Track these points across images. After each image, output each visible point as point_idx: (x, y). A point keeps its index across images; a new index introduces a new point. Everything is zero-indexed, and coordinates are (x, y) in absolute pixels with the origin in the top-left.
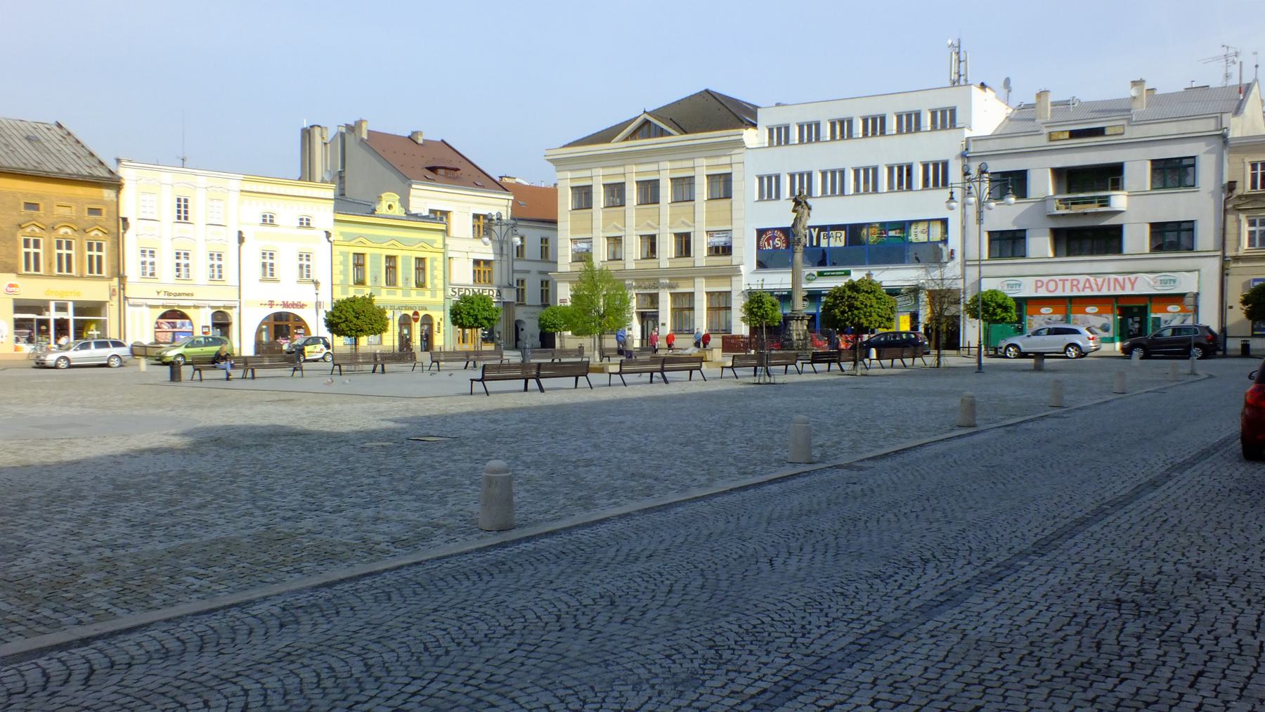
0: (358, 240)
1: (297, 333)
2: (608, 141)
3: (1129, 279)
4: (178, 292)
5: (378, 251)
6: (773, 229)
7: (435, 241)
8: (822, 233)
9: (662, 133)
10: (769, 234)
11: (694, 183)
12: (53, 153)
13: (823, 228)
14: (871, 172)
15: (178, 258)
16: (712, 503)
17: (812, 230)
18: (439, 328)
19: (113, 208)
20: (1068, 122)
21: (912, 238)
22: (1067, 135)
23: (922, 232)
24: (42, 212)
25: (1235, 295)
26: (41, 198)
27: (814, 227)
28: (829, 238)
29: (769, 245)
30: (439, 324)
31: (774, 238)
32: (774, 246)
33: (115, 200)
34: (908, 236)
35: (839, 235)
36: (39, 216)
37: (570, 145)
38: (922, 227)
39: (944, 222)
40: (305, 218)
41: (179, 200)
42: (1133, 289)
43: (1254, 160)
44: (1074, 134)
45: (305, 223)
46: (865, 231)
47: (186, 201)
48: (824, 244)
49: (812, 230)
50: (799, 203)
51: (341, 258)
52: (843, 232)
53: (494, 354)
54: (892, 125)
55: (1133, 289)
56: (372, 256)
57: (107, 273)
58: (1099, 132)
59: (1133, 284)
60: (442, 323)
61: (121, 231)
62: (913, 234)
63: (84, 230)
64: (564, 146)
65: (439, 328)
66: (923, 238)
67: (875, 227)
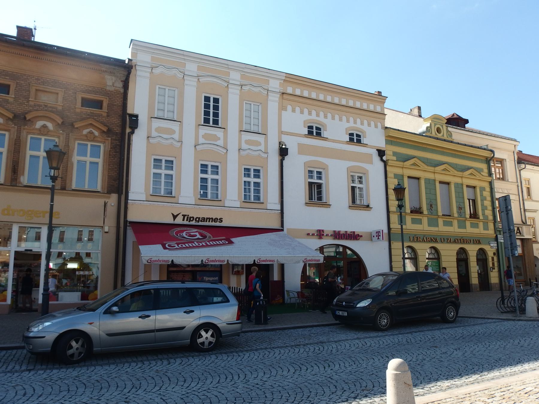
4: (201, 216)
15: (204, 171)
18: (493, 264)
19: (119, 102)
24: (12, 94)
26: (13, 76)
30: (493, 258)
33: (122, 91)
36: (7, 101)
40: (355, 133)
41: (207, 99)
47: (216, 101)
53: (44, 290)
56: (427, 181)
57: (102, 188)
61: (128, 130)
63: (72, 125)
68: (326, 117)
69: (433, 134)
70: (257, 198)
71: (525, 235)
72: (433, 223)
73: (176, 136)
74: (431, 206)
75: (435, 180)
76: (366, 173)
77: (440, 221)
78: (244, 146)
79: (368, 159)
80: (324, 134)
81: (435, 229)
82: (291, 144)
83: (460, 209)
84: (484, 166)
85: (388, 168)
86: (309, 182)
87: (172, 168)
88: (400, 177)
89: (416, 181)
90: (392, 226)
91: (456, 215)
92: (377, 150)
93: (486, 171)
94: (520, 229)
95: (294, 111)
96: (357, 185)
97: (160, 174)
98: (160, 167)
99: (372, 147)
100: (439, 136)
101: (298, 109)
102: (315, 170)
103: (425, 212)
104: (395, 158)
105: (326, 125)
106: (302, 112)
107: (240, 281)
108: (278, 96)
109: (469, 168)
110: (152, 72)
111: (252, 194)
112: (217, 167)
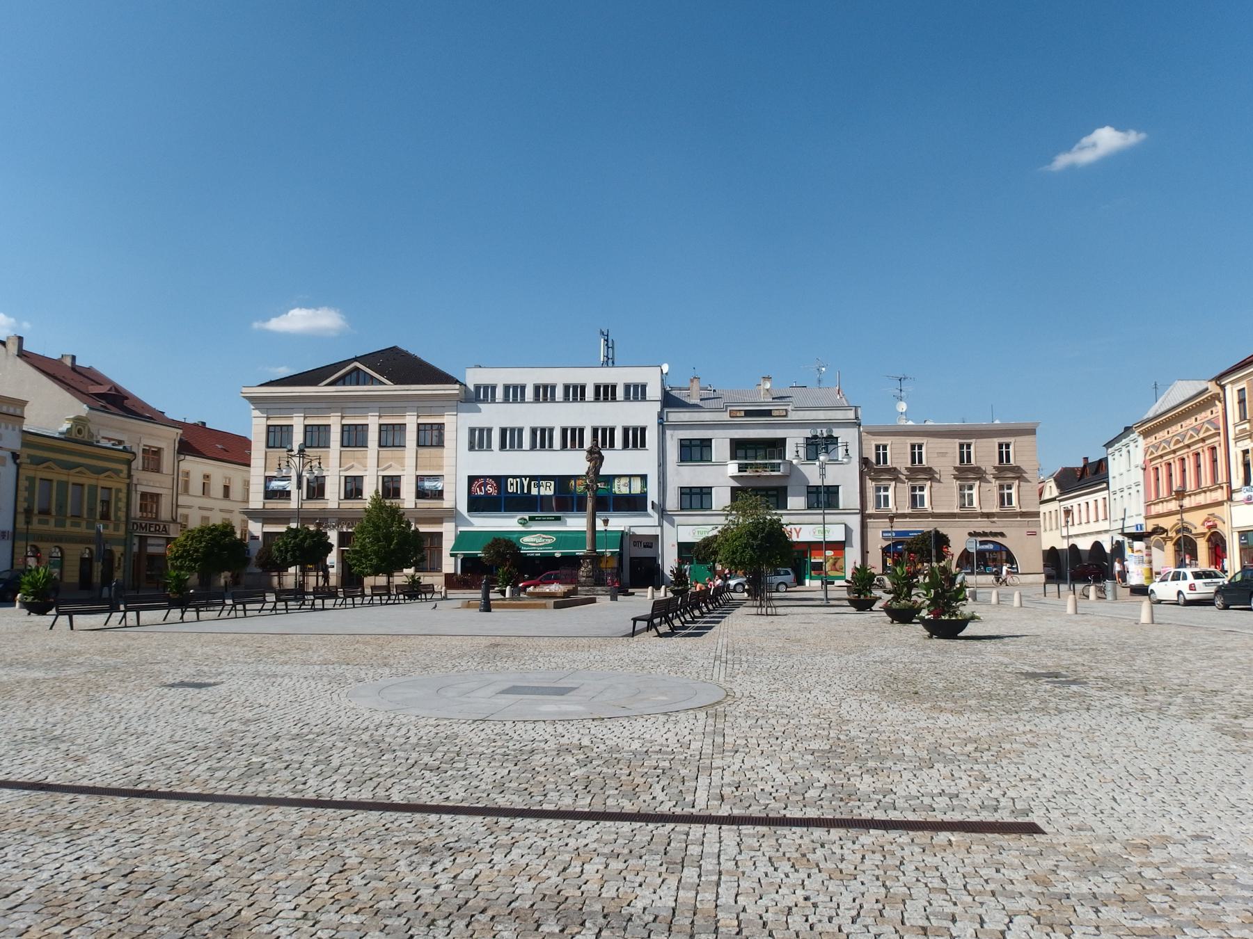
0: (45, 465)
1: (317, 576)
2: (315, 383)
3: (795, 529)
5: (64, 478)
7: (121, 471)
8: (533, 483)
10: (482, 481)
13: (532, 478)
14: (538, 433)
17: (523, 479)
18: (119, 564)
20: (744, 403)
21: (616, 490)
22: (743, 414)
23: (624, 486)
25: (877, 542)
27: (525, 477)
28: (539, 487)
29: (481, 490)
30: (120, 559)
31: (485, 485)
32: (486, 492)
35: (548, 484)
38: (624, 481)
39: (644, 478)
42: (798, 537)
43: (878, 443)
44: (748, 413)
46: (573, 482)
48: (534, 491)
49: (523, 479)
51: (26, 483)
52: (553, 483)
54: (590, 393)
55: (798, 537)
56: (59, 483)
58: (768, 413)
59: (798, 533)
60: (122, 559)
62: (616, 486)
65: (119, 564)
66: (625, 491)
69: (73, 436)
72: (60, 523)
74: (61, 507)
75: (97, 486)
77: (68, 522)
81: (62, 529)
83: (92, 510)
84: (124, 468)
85: (20, 470)
88: (31, 480)
90: (17, 526)
93: (125, 472)
100: (80, 437)
101: (10, 426)
103: (54, 513)
109: (107, 470)
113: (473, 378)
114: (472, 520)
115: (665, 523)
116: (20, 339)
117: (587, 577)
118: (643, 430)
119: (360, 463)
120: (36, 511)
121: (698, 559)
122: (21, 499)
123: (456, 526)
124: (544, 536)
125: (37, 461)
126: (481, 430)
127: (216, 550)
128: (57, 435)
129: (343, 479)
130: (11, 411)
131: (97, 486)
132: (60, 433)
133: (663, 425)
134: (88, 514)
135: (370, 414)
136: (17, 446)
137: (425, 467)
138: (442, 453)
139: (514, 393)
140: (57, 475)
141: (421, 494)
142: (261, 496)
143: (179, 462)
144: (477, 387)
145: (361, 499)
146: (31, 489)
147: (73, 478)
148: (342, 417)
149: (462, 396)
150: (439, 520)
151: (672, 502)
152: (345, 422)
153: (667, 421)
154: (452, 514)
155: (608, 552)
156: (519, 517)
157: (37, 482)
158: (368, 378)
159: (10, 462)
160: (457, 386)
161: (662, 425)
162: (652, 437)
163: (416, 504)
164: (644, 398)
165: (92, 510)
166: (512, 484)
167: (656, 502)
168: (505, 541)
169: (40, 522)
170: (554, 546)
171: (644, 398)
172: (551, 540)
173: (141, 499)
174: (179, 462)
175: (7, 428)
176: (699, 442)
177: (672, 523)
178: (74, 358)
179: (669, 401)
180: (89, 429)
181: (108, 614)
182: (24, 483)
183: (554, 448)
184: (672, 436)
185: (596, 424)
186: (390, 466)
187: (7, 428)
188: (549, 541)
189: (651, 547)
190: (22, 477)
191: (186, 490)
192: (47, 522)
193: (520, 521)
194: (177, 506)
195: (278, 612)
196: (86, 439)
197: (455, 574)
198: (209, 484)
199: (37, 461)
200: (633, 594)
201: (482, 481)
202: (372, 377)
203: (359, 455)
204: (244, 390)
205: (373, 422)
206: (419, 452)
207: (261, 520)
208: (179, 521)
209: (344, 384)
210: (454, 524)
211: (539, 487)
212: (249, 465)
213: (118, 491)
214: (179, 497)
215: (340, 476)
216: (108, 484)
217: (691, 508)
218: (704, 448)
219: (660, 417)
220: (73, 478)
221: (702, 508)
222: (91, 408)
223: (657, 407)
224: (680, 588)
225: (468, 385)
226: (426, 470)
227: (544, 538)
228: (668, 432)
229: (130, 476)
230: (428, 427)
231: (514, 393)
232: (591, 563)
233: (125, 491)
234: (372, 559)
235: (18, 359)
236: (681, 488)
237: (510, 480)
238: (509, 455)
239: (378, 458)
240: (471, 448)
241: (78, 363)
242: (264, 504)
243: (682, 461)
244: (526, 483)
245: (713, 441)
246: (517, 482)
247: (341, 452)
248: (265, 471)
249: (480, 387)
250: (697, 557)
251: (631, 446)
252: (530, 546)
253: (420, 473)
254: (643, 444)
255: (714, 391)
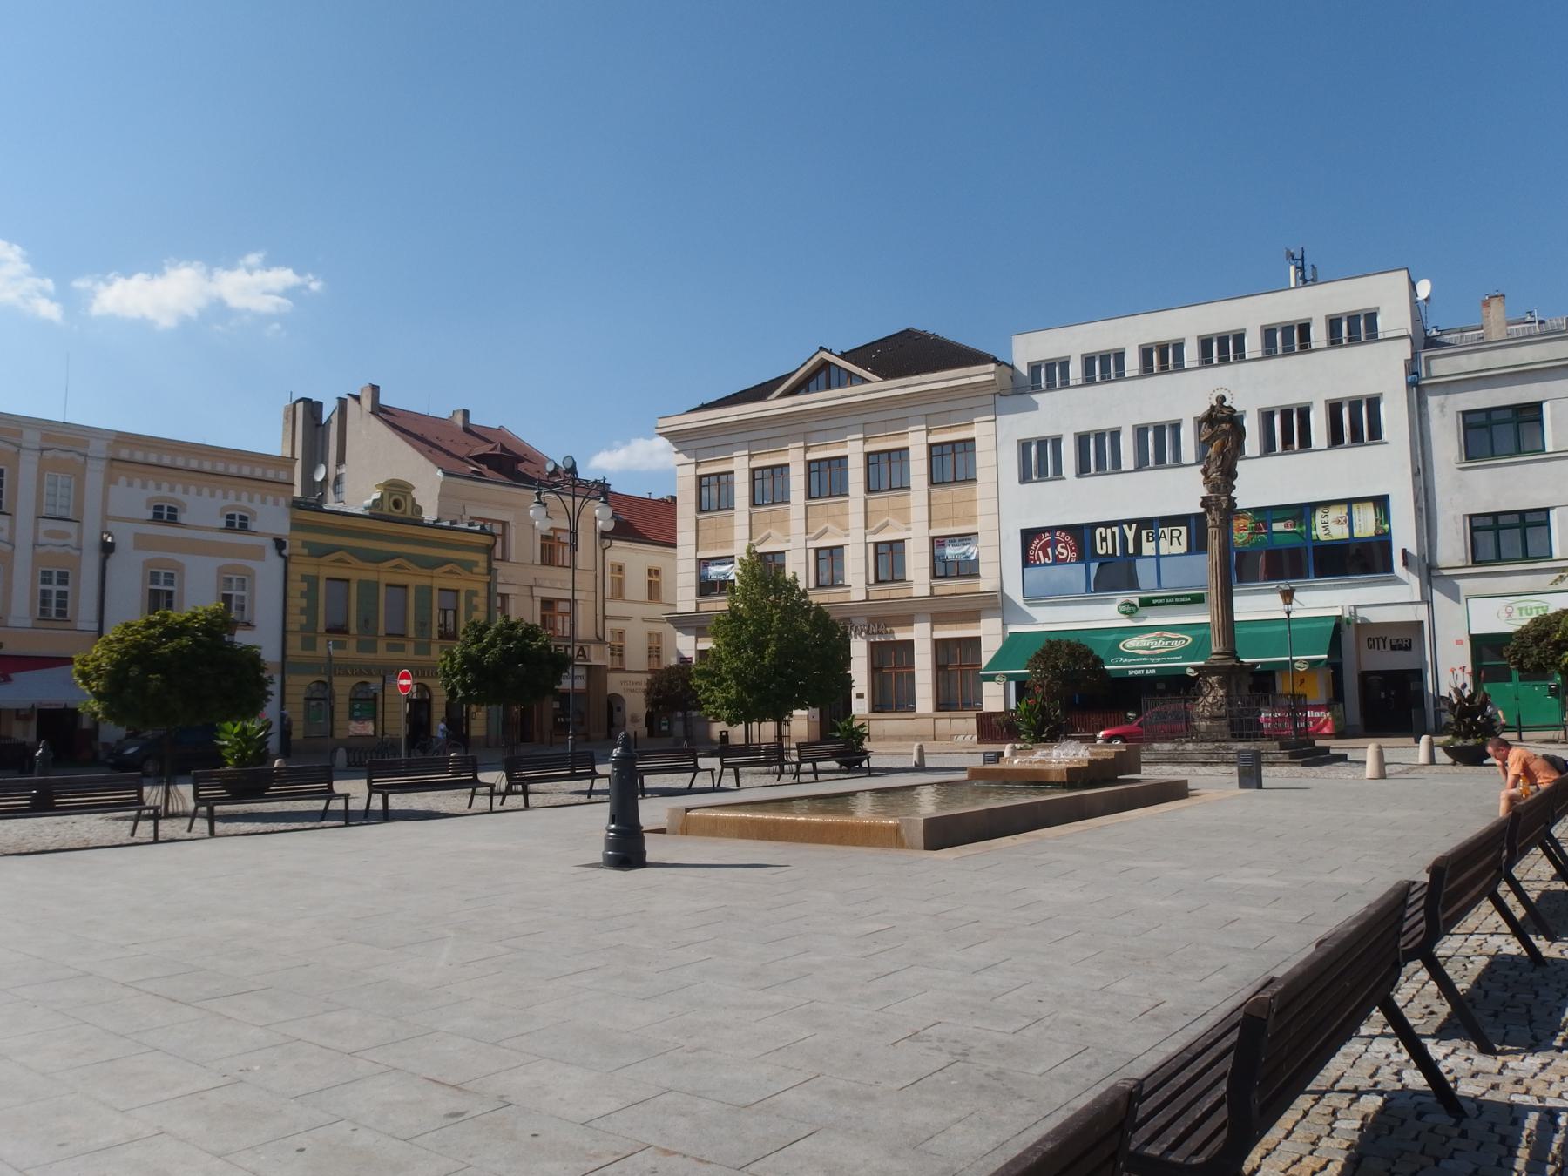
6: (1052, 529)
7: (476, 564)
8: (1144, 533)
9: (852, 378)
11: (974, 450)
12: (1400, 773)
13: (1144, 523)
14: (1277, 419)
16: (436, 747)
17: (1125, 527)
21: (1320, 533)
23: (1338, 522)
27: (1129, 522)
28: (1157, 539)
29: (1046, 555)
34: (1309, 529)
35: (1176, 533)
37: (704, 407)
38: (1336, 513)
39: (1381, 503)
40: (237, 513)
45: (237, 523)
49: (1125, 527)
50: (1222, 474)
52: (1184, 529)
54: (1319, 334)
56: (419, 589)
64: (689, 412)
66: (1339, 532)
67: (1247, 518)
68: (186, 491)
69: (386, 511)
70: (62, 613)
71: (592, 659)
72: (367, 646)
73: (72, 541)
74: (367, 623)
75: (431, 588)
76: (251, 574)
77: (381, 645)
78: (43, 539)
79: (258, 553)
80: (182, 518)
81: (372, 656)
82: (122, 535)
83: (423, 626)
84: (481, 558)
85: (291, 567)
86: (151, 590)
87: (66, 583)
88: (312, 581)
89: (345, 583)
90: (289, 652)
91: (412, 633)
92: (275, 539)
93: (483, 564)
94: (586, 649)
95: (130, 485)
96: (235, 593)
97: (50, 591)
98: (50, 582)
99: (264, 535)
100: (397, 512)
101: (270, 499)
102: (162, 572)
103: (353, 629)
104: (305, 551)
105: (185, 505)
106: (144, 486)
107: (898, 616)
108: (103, 463)
109: (447, 561)
110: (41, 458)
111: (54, 608)
112: (172, 576)
113: (1026, 350)
114: (1032, 611)
115: (1438, 597)
116: (375, 389)
117: (1214, 718)
118: (1374, 403)
119: (839, 525)
120: (321, 628)
121: (1521, 669)
122: (293, 609)
123: (1004, 625)
124: (1169, 635)
125: (319, 552)
126: (1042, 443)
127: (134, 671)
128: (360, 511)
129: (812, 554)
130: (271, 475)
131: (431, 588)
132: (366, 508)
133: (1418, 386)
134: (416, 630)
135: (849, 437)
136: (283, 528)
137: (944, 521)
138: (974, 491)
139: (1102, 367)
140: (358, 572)
141: (941, 568)
142: (693, 591)
143: (604, 550)
144: (1034, 368)
145: (842, 585)
146: (311, 594)
147: (386, 575)
148: (807, 449)
149: (1008, 384)
150: (973, 616)
151: (1452, 547)
152: (811, 456)
153: (1429, 377)
154: (996, 604)
155: (1301, 659)
156: (1119, 601)
157: (322, 584)
158: (844, 374)
159: (271, 552)
160: (992, 367)
161: (1418, 386)
162: (1394, 417)
163: (932, 588)
164: (1373, 336)
165: (423, 626)
166: (1104, 539)
167: (1413, 549)
168: (1069, 644)
169: (390, 648)
170: (1186, 653)
171: (1373, 336)
172: (1182, 641)
173: (543, 609)
174: (604, 550)
175: (264, 501)
176: (1508, 414)
177: (1454, 595)
178: (466, 413)
179: (1426, 342)
180: (414, 500)
181: (692, 774)
182: (297, 587)
183: (1184, 462)
184: (1442, 407)
185: (1269, 403)
186: (886, 525)
187: (264, 501)
188: (1178, 645)
189: (1408, 648)
190: (295, 576)
191: (619, 593)
192: (402, 648)
193: (1123, 608)
194: (605, 617)
195: (820, 777)
196: (409, 514)
197: (1007, 711)
198: (658, 583)
199: (319, 552)
200: (1175, 791)
201: (1046, 537)
202: (850, 374)
203: (834, 509)
204: (661, 423)
205: (854, 450)
206: (933, 494)
207: (693, 630)
208: (608, 639)
209: (808, 391)
210: (1000, 620)
211: (1157, 539)
212: (674, 546)
213: (471, 594)
214: (607, 604)
215: (807, 549)
216: (400, 579)
217: (1499, 559)
218: (1524, 427)
219: (1412, 368)
220: (386, 575)
221: (1526, 557)
222: (447, 474)
223: (1404, 350)
224: (1471, 742)
225: (1016, 365)
226: (948, 526)
227: (1170, 639)
228: (1433, 402)
229: (490, 570)
230: (948, 449)
231: (1102, 367)
232: (1221, 684)
233: (483, 593)
234: (730, 687)
235: (373, 419)
236: (1471, 517)
237: (1099, 530)
238: (1096, 484)
239: (866, 513)
240: (1025, 478)
241: (473, 420)
242: (697, 604)
243: (1469, 458)
244: (1130, 534)
245: (1546, 407)
246: (1113, 534)
247: (807, 507)
248: (697, 550)
249: (1039, 367)
250: (1520, 662)
251: (1347, 439)
252: (1138, 656)
253: (937, 532)
254: (1375, 434)
255: (1541, 322)
